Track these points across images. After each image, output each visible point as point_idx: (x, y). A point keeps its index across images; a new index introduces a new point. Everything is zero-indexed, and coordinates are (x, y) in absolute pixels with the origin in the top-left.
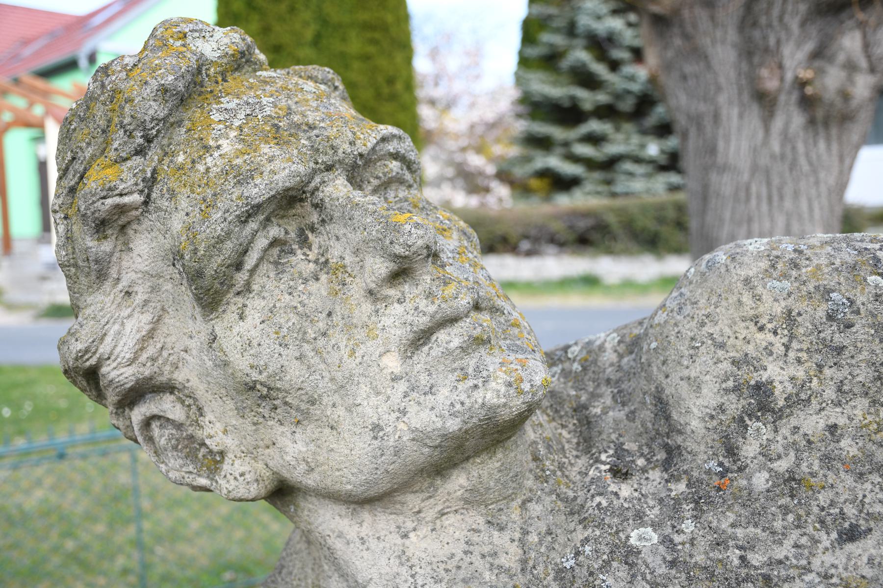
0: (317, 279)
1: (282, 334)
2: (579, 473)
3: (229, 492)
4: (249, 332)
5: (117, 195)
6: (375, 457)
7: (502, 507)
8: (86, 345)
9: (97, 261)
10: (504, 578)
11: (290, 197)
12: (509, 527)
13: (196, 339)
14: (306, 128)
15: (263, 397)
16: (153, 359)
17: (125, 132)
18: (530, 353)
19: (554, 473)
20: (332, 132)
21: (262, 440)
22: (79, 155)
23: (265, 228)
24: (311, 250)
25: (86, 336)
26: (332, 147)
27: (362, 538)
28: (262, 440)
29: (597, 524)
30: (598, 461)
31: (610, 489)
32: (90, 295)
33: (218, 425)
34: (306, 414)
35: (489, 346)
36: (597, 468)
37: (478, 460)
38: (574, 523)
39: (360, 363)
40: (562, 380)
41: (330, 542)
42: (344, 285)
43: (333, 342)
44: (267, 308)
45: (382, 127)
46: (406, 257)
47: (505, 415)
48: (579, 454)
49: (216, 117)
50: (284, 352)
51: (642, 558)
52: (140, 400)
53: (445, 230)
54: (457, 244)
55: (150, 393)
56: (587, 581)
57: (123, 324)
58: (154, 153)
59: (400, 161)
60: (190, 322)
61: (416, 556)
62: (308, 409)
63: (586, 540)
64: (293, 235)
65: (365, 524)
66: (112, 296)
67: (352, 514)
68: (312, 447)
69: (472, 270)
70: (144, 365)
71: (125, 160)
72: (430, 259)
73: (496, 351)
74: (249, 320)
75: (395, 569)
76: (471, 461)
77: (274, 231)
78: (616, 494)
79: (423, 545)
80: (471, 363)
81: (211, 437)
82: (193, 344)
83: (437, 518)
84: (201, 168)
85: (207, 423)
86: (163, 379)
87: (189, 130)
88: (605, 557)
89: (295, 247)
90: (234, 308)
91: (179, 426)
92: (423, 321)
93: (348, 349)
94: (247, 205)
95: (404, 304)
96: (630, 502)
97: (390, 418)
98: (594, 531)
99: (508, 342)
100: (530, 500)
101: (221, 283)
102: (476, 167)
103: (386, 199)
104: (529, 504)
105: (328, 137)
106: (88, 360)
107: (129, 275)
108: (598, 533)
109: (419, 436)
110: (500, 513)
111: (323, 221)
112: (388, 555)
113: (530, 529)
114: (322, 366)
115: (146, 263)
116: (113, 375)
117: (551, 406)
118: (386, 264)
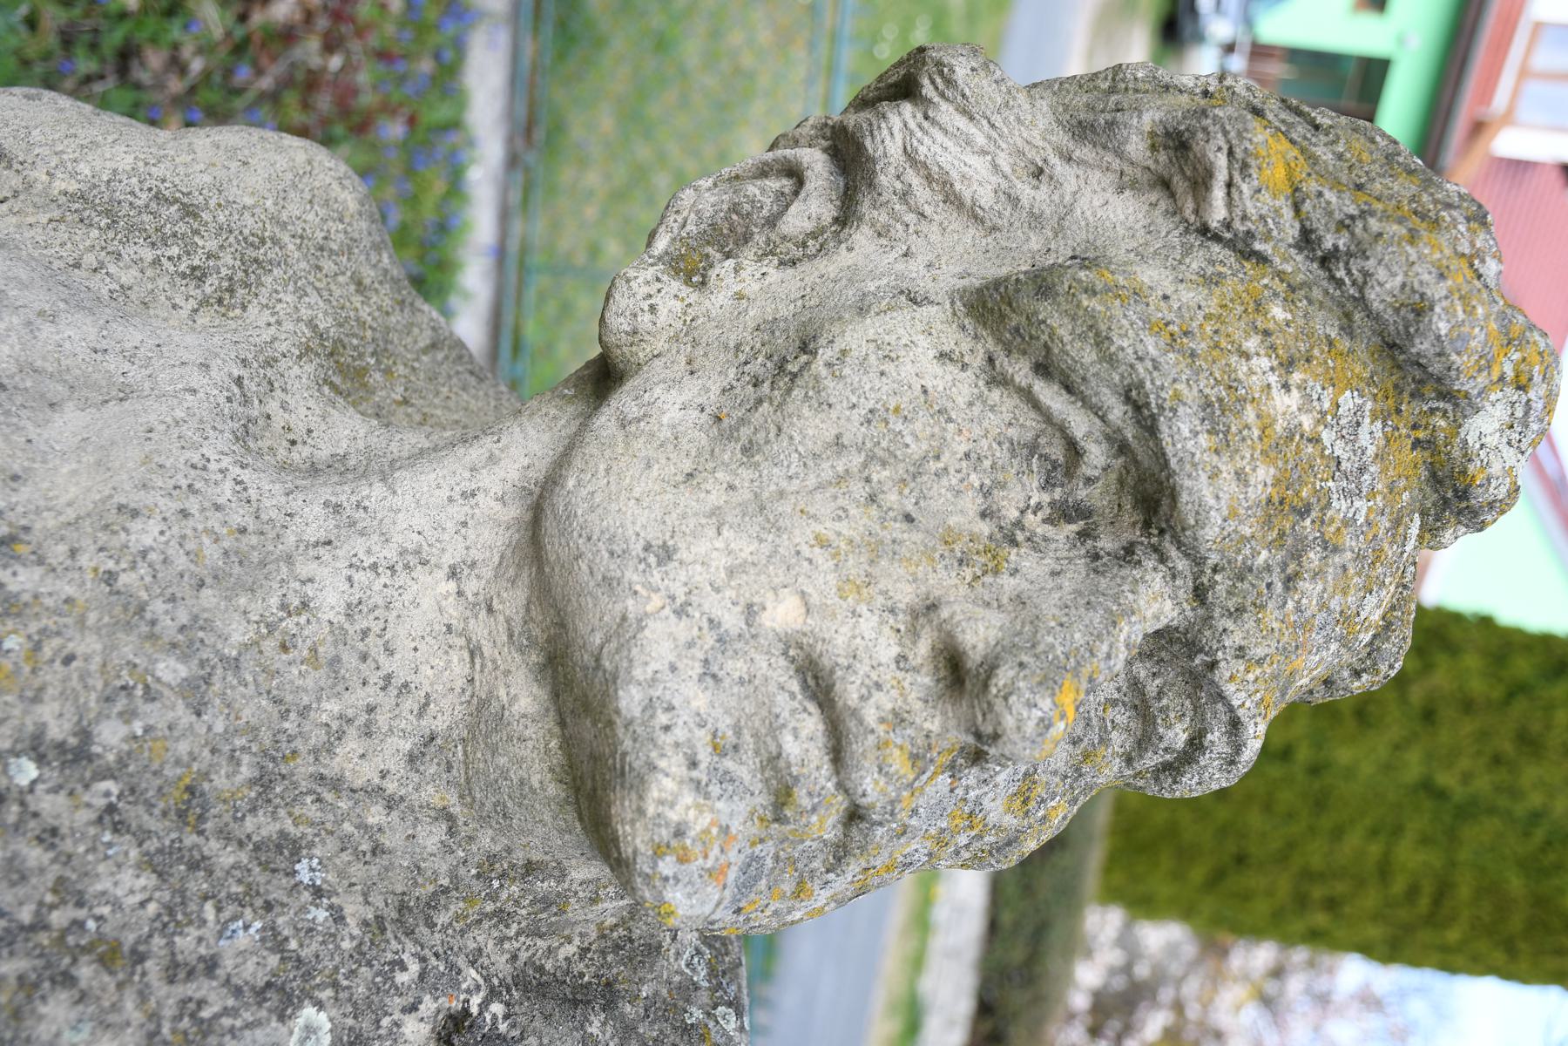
0: (983, 515)
1: (892, 418)
2: (480, 950)
3: (628, 281)
4: (911, 366)
5: (1231, 178)
6: (611, 540)
7: (454, 771)
8: (960, 82)
9: (1111, 124)
10: (318, 737)
11: (1158, 503)
12: (412, 775)
13: (923, 271)
14: (1289, 571)
15: (781, 367)
16: (905, 196)
17: (1352, 218)
18: (735, 900)
19: (493, 897)
20: (1271, 617)
21: (706, 355)
22: (1322, 137)
23: (1108, 438)
24: (1044, 521)
25: (977, 85)
26: (1240, 610)
27: (473, 495)
28: (706, 355)
29: (365, 949)
30: (493, 994)
31: (427, 998)
32: (1051, 107)
33: (756, 287)
34: (730, 435)
35: (769, 816)
36: (478, 988)
37: (553, 744)
38: (381, 905)
39: (798, 553)
40: (677, 978)
41: (488, 441)
42: (961, 562)
43: (853, 511)
44: (949, 405)
45: (1262, 728)
46: (986, 686)
47: (621, 808)
48: (520, 963)
49: (1348, 401)
50: (857, 415)
51: (269, 1020)
52: (838, 167)
53: (1025, 802)
54: (992, 819)
55: (846, 185)
56: (258, 893)
57: (984, 152)
58: (1298, 266)
59: (1185, 752)
60: (959, 269)
61: (410, 582)
62: (738, 440)
63: (338, 917)
64: (1082, 493)
65: (498, 506)
66: (1041, 143)
67: (524, 488)
68: (666, 433)
69: (933, 831)
70: (898, 177)
71: (1297, 208)
72: (971, 740)
73: (755, 829)
74: (936, 368)
75: (397, 538)
76: (557, 730)
77: (1096, 455)
78: (413, 1008)
79: (427, 603)
80: (744, 769)
81: (736, 271)
82: (916, 267)
83: (469, 640)
84: (1252, 344)
85: (764, 270)
86: (865, 208)
87: (1331, 344)
88: (293, 945)
89: (1058, 493)
90: (965, 346)
91: (772, 222)
92: (849, 692)
93: (832, 536)
94: (1161, 407)
95: (893, 666)
96: (391, 1033)
97: (678, 584)
98: (352, 938)
99: (769, 862)
100: (451, 832)
101: (1017, 330)
102: (1144, 1022)
103: (1114, 703)
104: (444, 827)
105: (1262, 607)
106: (933, 82)
107: (1073, 180)
108: (346, 945)
109: (625, 630)
110: (443, 766)
111: (1096, 557)
112: (428, 533)
113: (395, 814)
114: (812, 481)
115: (1088, 213)
116: (895, 120)
117: (631, 941)
118: (981, 646)
